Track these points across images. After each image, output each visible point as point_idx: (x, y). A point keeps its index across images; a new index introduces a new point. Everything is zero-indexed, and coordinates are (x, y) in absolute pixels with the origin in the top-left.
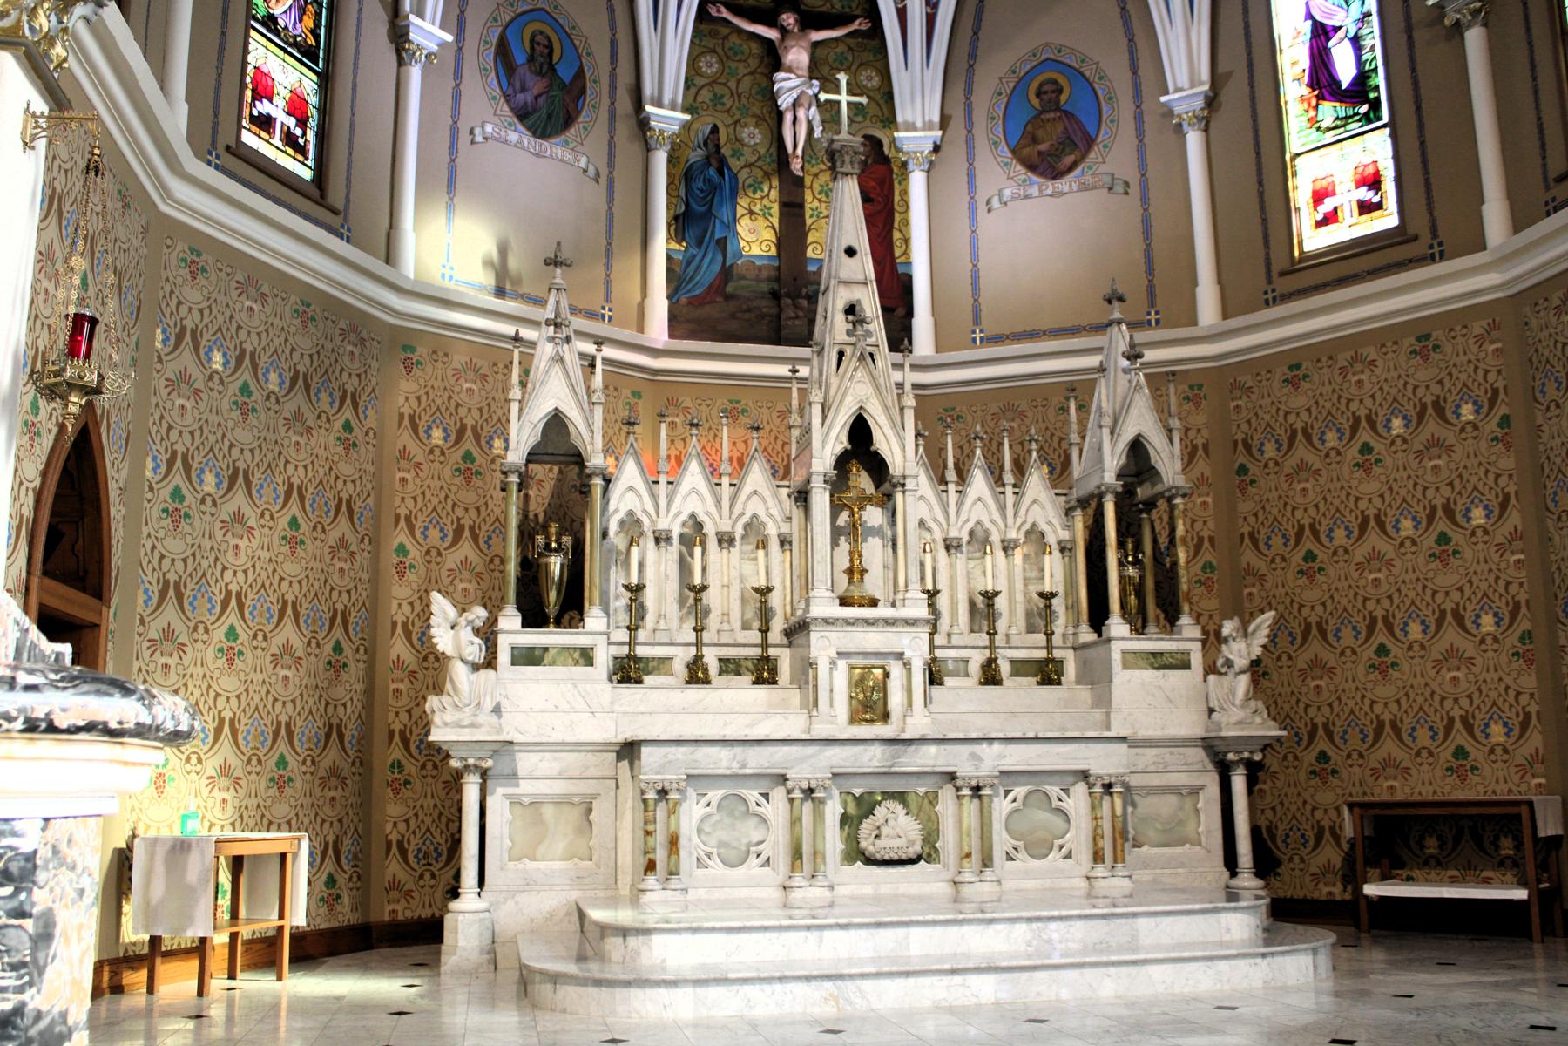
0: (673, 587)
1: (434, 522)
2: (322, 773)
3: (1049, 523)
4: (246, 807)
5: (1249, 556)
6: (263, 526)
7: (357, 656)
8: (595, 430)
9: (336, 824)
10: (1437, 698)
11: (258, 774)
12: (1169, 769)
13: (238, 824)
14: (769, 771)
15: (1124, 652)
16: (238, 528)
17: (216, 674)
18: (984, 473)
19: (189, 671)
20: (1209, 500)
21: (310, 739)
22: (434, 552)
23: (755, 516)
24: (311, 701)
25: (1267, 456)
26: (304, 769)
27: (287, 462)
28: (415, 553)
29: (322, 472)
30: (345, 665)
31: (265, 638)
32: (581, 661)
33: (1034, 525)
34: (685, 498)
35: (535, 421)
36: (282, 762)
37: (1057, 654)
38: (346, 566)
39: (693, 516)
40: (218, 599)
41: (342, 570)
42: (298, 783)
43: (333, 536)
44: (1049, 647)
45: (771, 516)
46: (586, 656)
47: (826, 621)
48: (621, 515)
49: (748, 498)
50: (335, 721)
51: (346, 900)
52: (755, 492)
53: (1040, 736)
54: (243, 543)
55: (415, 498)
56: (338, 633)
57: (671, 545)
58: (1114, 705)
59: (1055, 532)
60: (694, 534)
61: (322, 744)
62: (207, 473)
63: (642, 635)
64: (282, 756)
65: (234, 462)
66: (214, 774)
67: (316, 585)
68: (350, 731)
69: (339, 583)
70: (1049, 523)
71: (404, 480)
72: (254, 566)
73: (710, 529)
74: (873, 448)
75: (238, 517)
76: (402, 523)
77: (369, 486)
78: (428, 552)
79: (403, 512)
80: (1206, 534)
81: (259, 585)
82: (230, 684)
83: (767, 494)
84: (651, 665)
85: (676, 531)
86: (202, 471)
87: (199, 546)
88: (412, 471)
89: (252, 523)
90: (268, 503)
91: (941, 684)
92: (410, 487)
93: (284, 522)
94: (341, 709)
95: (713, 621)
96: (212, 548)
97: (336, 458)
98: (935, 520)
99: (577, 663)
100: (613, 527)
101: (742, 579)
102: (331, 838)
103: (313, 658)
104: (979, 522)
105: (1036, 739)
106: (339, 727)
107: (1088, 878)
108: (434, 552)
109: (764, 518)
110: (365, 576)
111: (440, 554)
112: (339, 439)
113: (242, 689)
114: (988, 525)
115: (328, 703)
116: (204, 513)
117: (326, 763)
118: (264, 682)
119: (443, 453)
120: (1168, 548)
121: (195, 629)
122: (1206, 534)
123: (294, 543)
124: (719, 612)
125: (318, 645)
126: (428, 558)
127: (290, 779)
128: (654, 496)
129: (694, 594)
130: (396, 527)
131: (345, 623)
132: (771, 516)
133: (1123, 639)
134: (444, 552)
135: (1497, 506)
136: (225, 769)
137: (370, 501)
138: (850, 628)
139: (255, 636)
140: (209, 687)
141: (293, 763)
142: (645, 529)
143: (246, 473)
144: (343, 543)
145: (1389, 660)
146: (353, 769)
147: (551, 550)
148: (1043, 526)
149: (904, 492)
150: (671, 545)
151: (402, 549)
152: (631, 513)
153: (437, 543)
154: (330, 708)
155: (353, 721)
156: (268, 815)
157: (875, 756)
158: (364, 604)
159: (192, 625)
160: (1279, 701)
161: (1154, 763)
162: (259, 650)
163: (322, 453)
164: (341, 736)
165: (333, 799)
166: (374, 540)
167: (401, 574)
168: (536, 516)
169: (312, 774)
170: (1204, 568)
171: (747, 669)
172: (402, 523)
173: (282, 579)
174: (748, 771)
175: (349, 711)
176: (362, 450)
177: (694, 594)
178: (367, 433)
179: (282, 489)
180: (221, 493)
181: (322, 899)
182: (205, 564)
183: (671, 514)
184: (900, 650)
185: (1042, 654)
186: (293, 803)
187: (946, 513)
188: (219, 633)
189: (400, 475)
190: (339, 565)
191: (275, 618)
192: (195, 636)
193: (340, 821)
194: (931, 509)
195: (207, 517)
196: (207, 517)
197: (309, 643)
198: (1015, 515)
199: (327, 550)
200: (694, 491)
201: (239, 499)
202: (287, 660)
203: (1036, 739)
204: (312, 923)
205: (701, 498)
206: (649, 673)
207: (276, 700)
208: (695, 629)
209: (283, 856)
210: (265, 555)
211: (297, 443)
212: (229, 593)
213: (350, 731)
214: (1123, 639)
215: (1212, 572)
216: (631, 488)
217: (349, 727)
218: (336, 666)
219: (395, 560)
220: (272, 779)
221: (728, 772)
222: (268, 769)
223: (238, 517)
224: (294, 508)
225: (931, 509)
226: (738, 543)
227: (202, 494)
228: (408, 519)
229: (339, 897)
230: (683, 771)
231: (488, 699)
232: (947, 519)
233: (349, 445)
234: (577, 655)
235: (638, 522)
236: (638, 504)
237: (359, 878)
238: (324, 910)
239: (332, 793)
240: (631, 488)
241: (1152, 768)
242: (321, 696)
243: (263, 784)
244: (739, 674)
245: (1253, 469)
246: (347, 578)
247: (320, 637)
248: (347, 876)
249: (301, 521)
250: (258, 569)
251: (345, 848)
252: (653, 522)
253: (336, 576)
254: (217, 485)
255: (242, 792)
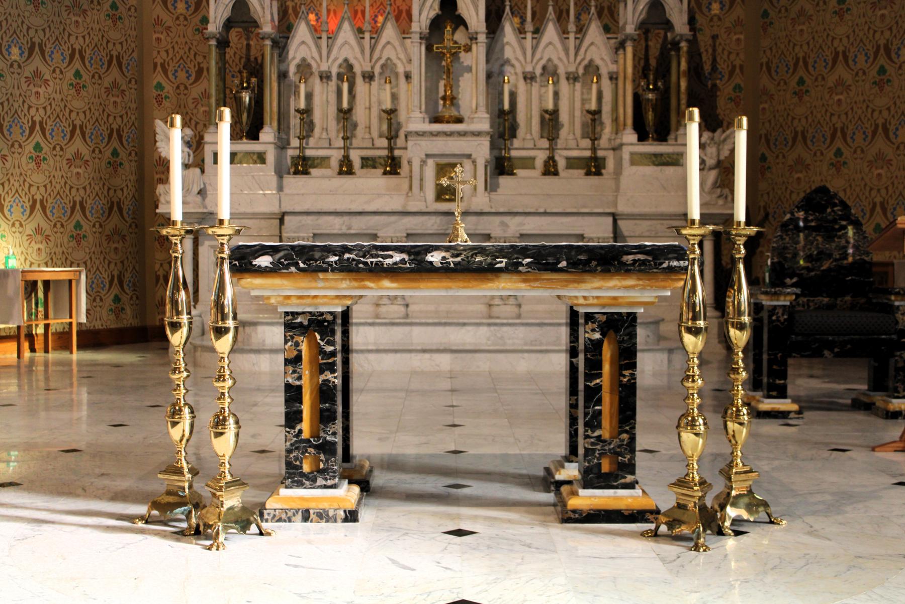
0: (333, 110)
1: (182, 66)
2: (107, 232)
3: (602, 59)
4: (55, 253)
5: (765, 81)
6: (55, 78)
7: (130, 158)
8: (266, 8)
9: (119, 265)
10: (868, 189)
11: (62, 233)
12: (660, 234)
13: (49, 263)
14: (366, 232)
15: (632, 154)
16: (38, 81)
17: (29, 172)
18: (554, 25)
19: (10, 172)
20: (742, 37)
21: (97, 212)
22: (182, 88)
23: (389, 59)
24: (97, 188)
25: (713, 12)
26: (94, 230)
27: (70, 35)
28: (168, 88)
29: (96, 39)
30: (121, 164)
31: (62, 149)
32: (258, 161)
33: (591, 61)
34: (340, 48)
35: (227, 3)
36: (78, 226)
37: (600, 153)
38: (118, 100)
39: (346, 60)
40: (27, 127)
41: (115, 102)
42: (91, 239)
43: (107, 81)
44: (594, 149)
45: (399, 59)
46: (261, 158)
47: (418, 134)
48: (297, 61)
49: (384, 47)
50: (115, 200)
51: (128, 311)
52: (388, 43)
53: (548, 211)
54: (41, 90)
55: (167, 51)
56: (115, 143)
57: (331, 81)
58: (621, 191)
59: (607, 65)
60: (347, 72)
61: (106, 214)
62: (13, 47)
63: (312, 141)
64: (78, 222)
65: (31, 39)
66: (32, 233)
67: (97, 114)
68: (127, 205)
69: (114, 111)
70: (602, 59)
71: (159, 39)
72: (50, 104)
73: (357, 70)
74: (440, 13)
75: (37, 74)
76: (159, 68)
77: (133, 45)
78: (178, 87)
79: (159, 61)
80: (738, 63)
81: (55, 116)
82: (38, 178)
83: (397, 43)
84: (316, 162)
85: (334, 71)
86: (10, 46)
87: (11, 94)
88: (165, 33)
89: (47, 77)
90: (58, 63)
91: (512, 174)
92: (163, 43)
93: (70, 74)
94: (119, 193)
95: (360, 131)
96: (20, 95)
97: (106, 29)
98: (517, 59)
99: (255, 162)
100: (292, 69)
101: (380, 103)
102: (116, 273)
103: (97, 160)
104: (550, 60)
105: (545, 214)
106: (119, 204)
107: (490, 305)
108: (182, 88)
109: (395, 61)
110: (134, 106)
111: (186, 88)
112: (108, 15)
113: (47, 181)
114: (556, 61)
115: (109, 189)
116: (13, 73)
117: (110, 227)
118: (62, 176)
119: (186, 19)
120: (710, 74)
121: (13, 145)
122: (738, 63)
123: (78, 88)
124: (364, 126)
125: (100, 152)
126: (178, 91)
127: (85, 236)
128: (319, 48)
129: (345, 115)
130: (154, 71)
131: (120, 137)
132: (399, 59)
133: (632, 144)
134: (189, 87)
135: (727, 73)
136: (38, 230)
137: (135, 55)
138: (434, 138)
139: (54, 148)
140: (25, 180)
141: (86, 226)
142: (314, 70)
143: (40, 45)
144: (115, 84)
145: (842, 160)
146: (130, 230)
147: (243, 88)
148: (598, 62)
149: (477, 43)
150: (331, 81)
151: (159, 86)
152: (304, 60)
153: (185, 81)
154: (112, 192)
155: (129, 199)
156: (70, 258)
157: (436, 223)
158: (133, 124)
159: (10, 143)
160: (896, 182)
161: (648, 231)
162: (58, 157)
163: (96, 26)
164: (120, 210)
165: (116, 248)
166: (140, 82)
167: (160, 103)
168: (256, 59)
169: (100, 233)
170: (735, 89)
171: (381, 164)
172: (159, 68)
173: (71, 111)
174: (352, 232)
175: (125, 193)
176: (127, 22)
177: (345, 115)
178: (129, 9)
179: (67, 53)
180: (24, 59)
181: (111, 310)
182: (16, 105)
183: (330, 60)
184: (469, 153)
185: (588, 154)
186: (88, 251)
187: (524, 54)
188: (29, 148)
189: (155, 36)
190: (113, 99)
191: (68, 136)
192: (13, 150)
193: (122, 262)
194: (514, 52)
195: (16, 75)
196: (16, 75)
197: (94, 151)
198: (576, 55)
199: (103, 90)
200: (346, 43)
201: (37, 62)
202: (78, 162)
203: (545, 214)
204: (104, 324)
205: (352, 47)
206: (315, 167)
207: (71, 188)
208: (343, 138)
209: (70, 281)
210: (58, 97)
211: (77, 22)
212: (34, 123)
213: (127, 205)
214: (632, 144)
215: (740, 92)
216: (303, 42)
217: (126, 203)
218: (114, 165)
219: (155, 93)
220: (72, 236)
221: (340, 232)
222: (69, 230)
223: (37, 74)
224: (77, 64)
225: (514, 52)
226: (376, 78)
227: (10, 61)
228: (163, 65)
229: (123, 309)
230: (311, 231)
231: (195, 186)
232: (525, 58)
233: (115, 19)
234: (255, 157)
235: (309, 66)
236: (309, 53)
237: (137, 298)
238: (112, 317)
239: (115, 245)
240: (303, 42)
241: (647, 234)
242: (104, 184)
243: (66, 240)
244: (374, 167)
245: (772, 14)
246: (119, 108)
247: (102, 146)
248: (129, 297)
249: (82, 72)
250: (54, 106)
251: (128, 276)
252: (319, 66)
253: (111, 107)
254: (21, 55)
255: (51, 244)
